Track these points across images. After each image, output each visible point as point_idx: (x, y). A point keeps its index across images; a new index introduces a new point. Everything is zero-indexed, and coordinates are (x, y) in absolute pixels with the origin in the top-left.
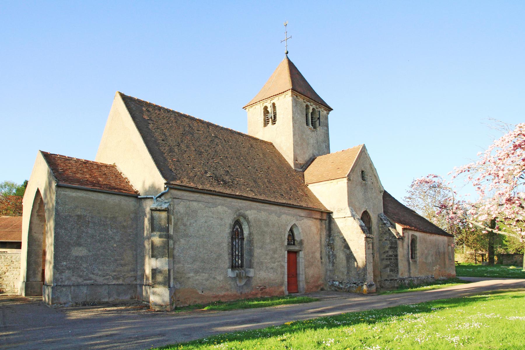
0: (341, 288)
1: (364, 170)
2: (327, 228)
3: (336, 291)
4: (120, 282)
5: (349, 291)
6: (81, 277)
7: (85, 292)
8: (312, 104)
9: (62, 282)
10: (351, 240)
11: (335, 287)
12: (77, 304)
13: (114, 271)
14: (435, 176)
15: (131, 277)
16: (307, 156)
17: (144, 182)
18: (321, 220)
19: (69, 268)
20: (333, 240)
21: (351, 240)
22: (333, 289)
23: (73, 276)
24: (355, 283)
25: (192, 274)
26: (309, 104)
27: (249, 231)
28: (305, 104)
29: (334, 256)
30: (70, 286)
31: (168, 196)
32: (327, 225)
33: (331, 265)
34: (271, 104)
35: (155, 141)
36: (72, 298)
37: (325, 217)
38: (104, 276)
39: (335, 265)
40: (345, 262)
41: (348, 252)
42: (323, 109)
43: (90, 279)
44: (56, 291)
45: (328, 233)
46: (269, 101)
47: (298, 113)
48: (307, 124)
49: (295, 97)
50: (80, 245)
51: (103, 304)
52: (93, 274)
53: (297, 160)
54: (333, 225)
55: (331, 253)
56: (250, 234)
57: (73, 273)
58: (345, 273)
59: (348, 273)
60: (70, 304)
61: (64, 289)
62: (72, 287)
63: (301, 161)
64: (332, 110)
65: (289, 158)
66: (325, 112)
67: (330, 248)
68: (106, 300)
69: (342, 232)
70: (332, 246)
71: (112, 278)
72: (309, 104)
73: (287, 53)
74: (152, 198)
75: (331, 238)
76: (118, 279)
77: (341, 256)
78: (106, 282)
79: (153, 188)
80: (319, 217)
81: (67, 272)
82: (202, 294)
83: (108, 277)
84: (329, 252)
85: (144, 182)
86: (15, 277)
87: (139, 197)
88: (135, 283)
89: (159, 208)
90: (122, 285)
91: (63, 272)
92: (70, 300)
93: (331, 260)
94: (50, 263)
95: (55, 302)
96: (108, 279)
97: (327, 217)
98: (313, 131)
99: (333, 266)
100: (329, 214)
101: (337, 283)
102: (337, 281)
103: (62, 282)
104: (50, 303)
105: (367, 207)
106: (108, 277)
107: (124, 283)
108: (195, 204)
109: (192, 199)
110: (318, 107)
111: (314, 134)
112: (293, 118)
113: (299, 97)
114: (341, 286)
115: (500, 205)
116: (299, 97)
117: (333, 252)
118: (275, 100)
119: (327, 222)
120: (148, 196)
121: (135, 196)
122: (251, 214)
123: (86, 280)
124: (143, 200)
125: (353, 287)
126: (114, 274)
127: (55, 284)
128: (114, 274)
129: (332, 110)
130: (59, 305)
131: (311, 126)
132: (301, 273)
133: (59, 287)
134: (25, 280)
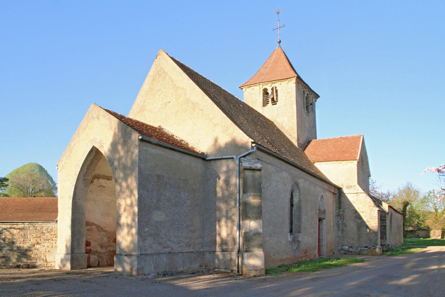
0: (352, 252)
2: (337, 201)
3: (345, 254)
4: (192, 250)
5: (359, 254)
6: (160, 244)
7: (165, 260)
9: (145, 250)
10: (363, 212)
11: (345, 251)
12: (158, 274)
13: (186, 238)
15: (199, 244)
17: (216, 140)
18: (334, 194)
19: (151, 235)
20: (343, 211)
21: (363, 212)
22: (342, 252)
23: (154, 243)
24: (366, 247)
25: (267, 238)
26: (305, 90)
27: (300, 198)
28: (303, 90)
29: (345, 225)
30: (152, 255)
31: (254, 156)
32: (337, 198)
33: (340, 232)
34: (271, 88)
36: (154, 268)
37: (336, 192)
38: (179, 244)
39: (344, 232)
40: (355, 230)
41: (359, 221)
43: (167, 247)
44: (141, 260)
45: (338, 205)
46: (270, 85)
50: (158, 208)
51: (179, 273)
52: (170, 241)
54: (343, 199)
55: (340, 222)
56: (300, 201)
57: (154, 240)
58: (356, 238)
59: (359, 238)
60: (153, 274)
61: (148, 258)
62: (154, 255)
65: (294, 140)
67: (339, 218)
68: (181, 269)
69: (354, 204)
70: (342, 217)
71: (185, 245)
73: (280, 42)
74: (233, 158)
75: (341, 210)
76: (189, 246)
77: (352, 225)
78: (180, 250)
79: (234, 145)
80: (333, 191)
81: (149, 239)
82: (274, 257)
83: (182, 244)
84: (338, 221)
85: (216, 140)
86: (48, 249)
87: (207, 158)
88: (202, 250)
89: (253, 167)
90: (192, 252)
91: (146, 239)
92: (153, 270)
93: (341, 228)
94: (130, 227)
95: (140, 273)
96: (182, 246)
97: (338, 192)
99: (342, 233)
100: (339, 189)
101: (347, 247)
102: (346, 245)
103: (145, 250)
104: (134, 273)
106: (182, 244)
107: (194, 251)
108: (270, 167)
109: (268, 161)
114: (351, 250)
117: (342, 222)
118: (277, 85)
119: (337, 196)
120: (224, 157)
121: (202, 157)
122: (301, 182)
123: (164, 248)
124: (213, 162)
125: (364, 250)
126: (187, 240)
127: (140, 253)
128: (187, 240)
130: (144, 276)
132: (324, 238)
133: (143, 256)
134: (70, 251)
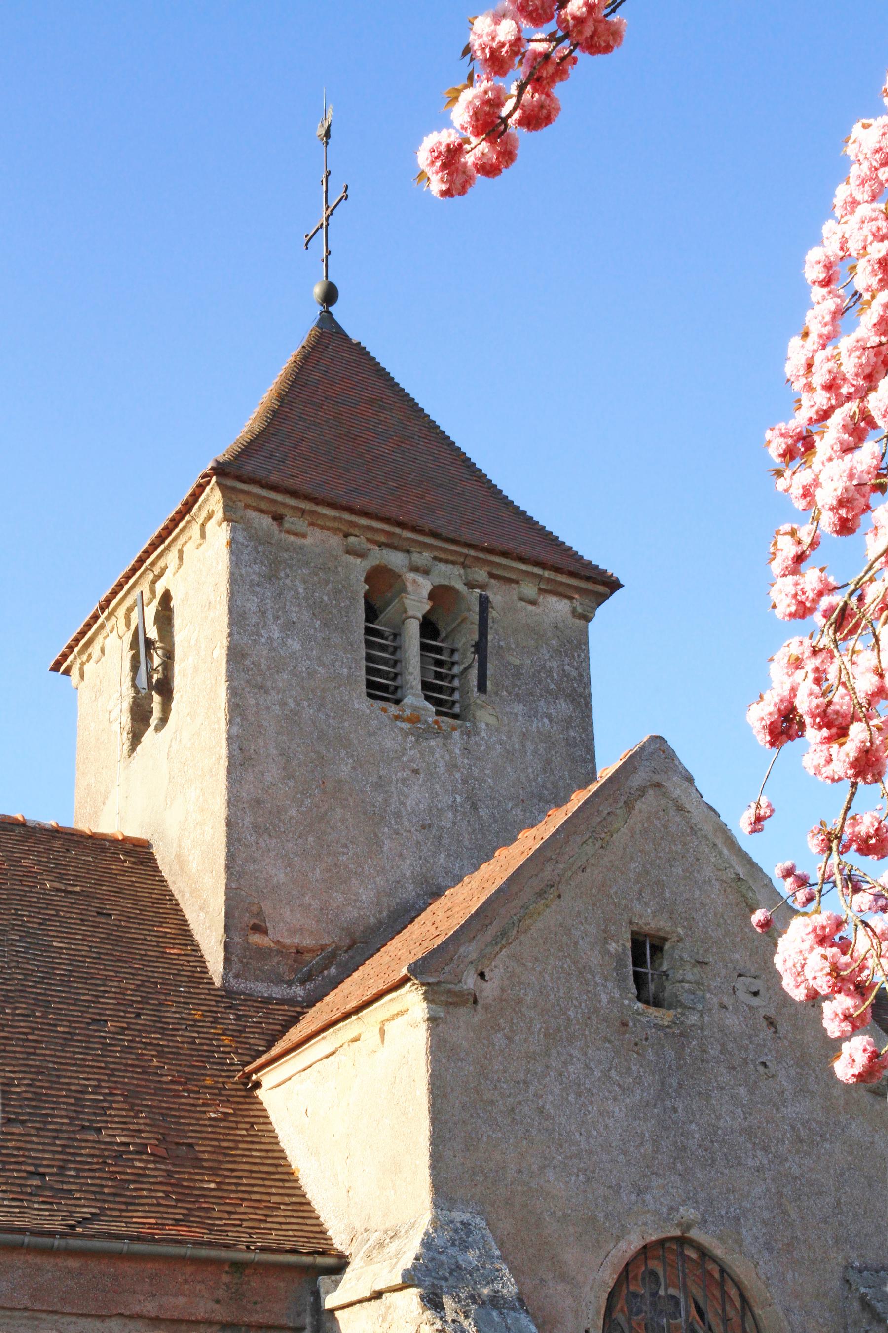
1: (651, 920)
8: (424, 558)
14: (759, 819)
16: (366, 895)
28: (359, 567)
35: (313, 991)
42: (529, 589)
47: (289, 626)
48: (382, 688)
49: (266, 521)
53: (258, 929)
63: (294, 925)
64: (614, 585)
66: (558, 608)
72: (396, 560)
98: (436, 731)
105: (689, 1213)
110: (481, 575)
111: (444, 751)
112: (235, 655)
113: (292, 521)
115: (698, 962)
116: (292, 521)
129: (614, 585)
131: (414, 698)
